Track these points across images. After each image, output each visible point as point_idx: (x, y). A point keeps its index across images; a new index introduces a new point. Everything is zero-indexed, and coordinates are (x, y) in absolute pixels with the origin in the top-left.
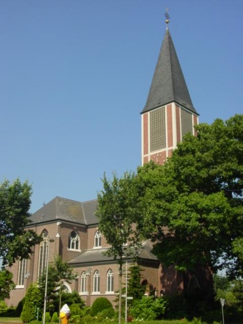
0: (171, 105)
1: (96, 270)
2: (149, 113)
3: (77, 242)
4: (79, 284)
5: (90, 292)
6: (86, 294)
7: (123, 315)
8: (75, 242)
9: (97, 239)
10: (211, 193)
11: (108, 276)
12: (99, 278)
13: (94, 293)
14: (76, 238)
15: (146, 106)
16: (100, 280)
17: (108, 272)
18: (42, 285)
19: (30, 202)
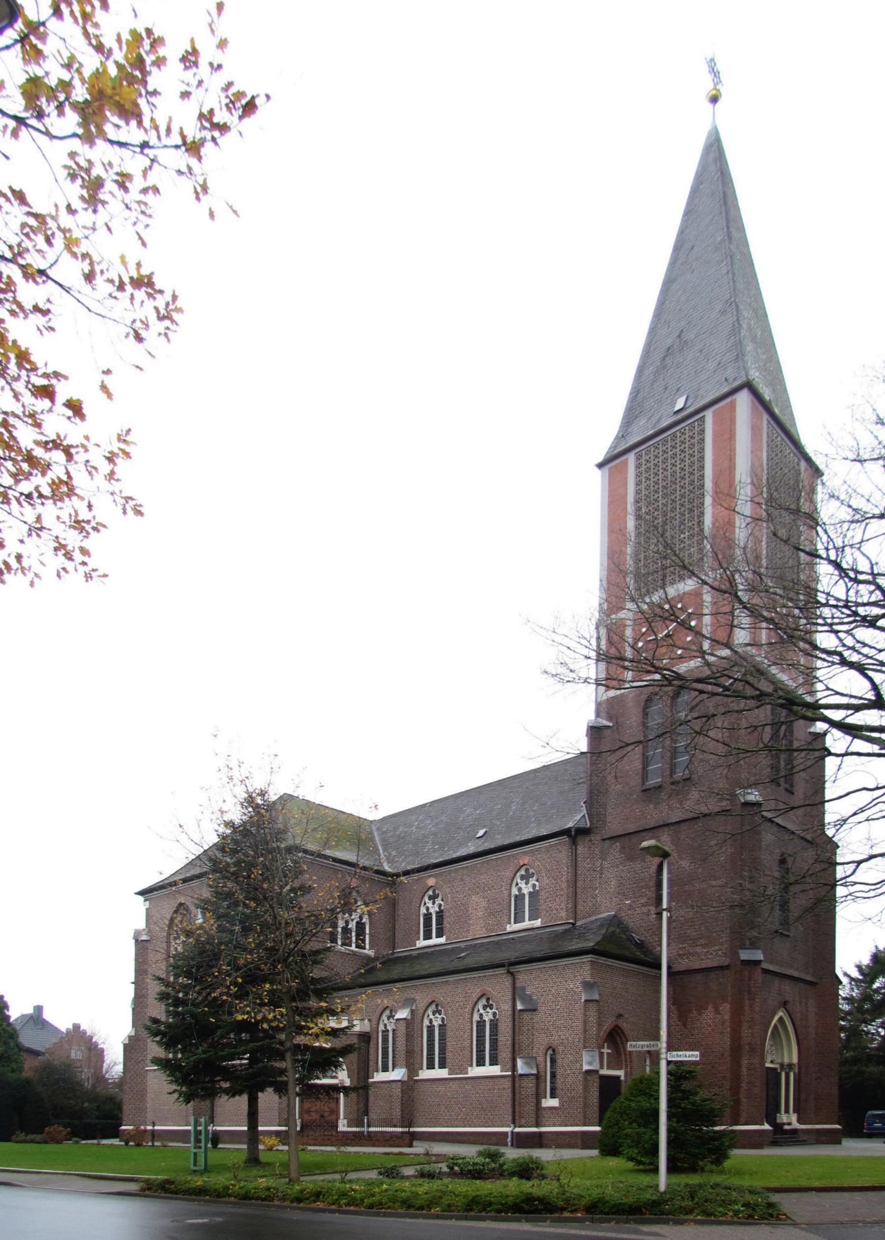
0: (735, 400)
1: (433, 1001)
2: (631, 457)
3: (360, 926)
4: (372, 1051)
5: (412, 1070)
6: (398, 1078)
7: (538, 1141)
8: (352, 925)
9: (428, 917)
10: (630, 1223)
11: (476, 1017)
12: (442, 1027)
13: (425, 1074)
14: (355, 916)
15: (622, 435)
16: (449, 1034)
17: (476, 1003)
18: (290, 964)
19: (102, 1051)
